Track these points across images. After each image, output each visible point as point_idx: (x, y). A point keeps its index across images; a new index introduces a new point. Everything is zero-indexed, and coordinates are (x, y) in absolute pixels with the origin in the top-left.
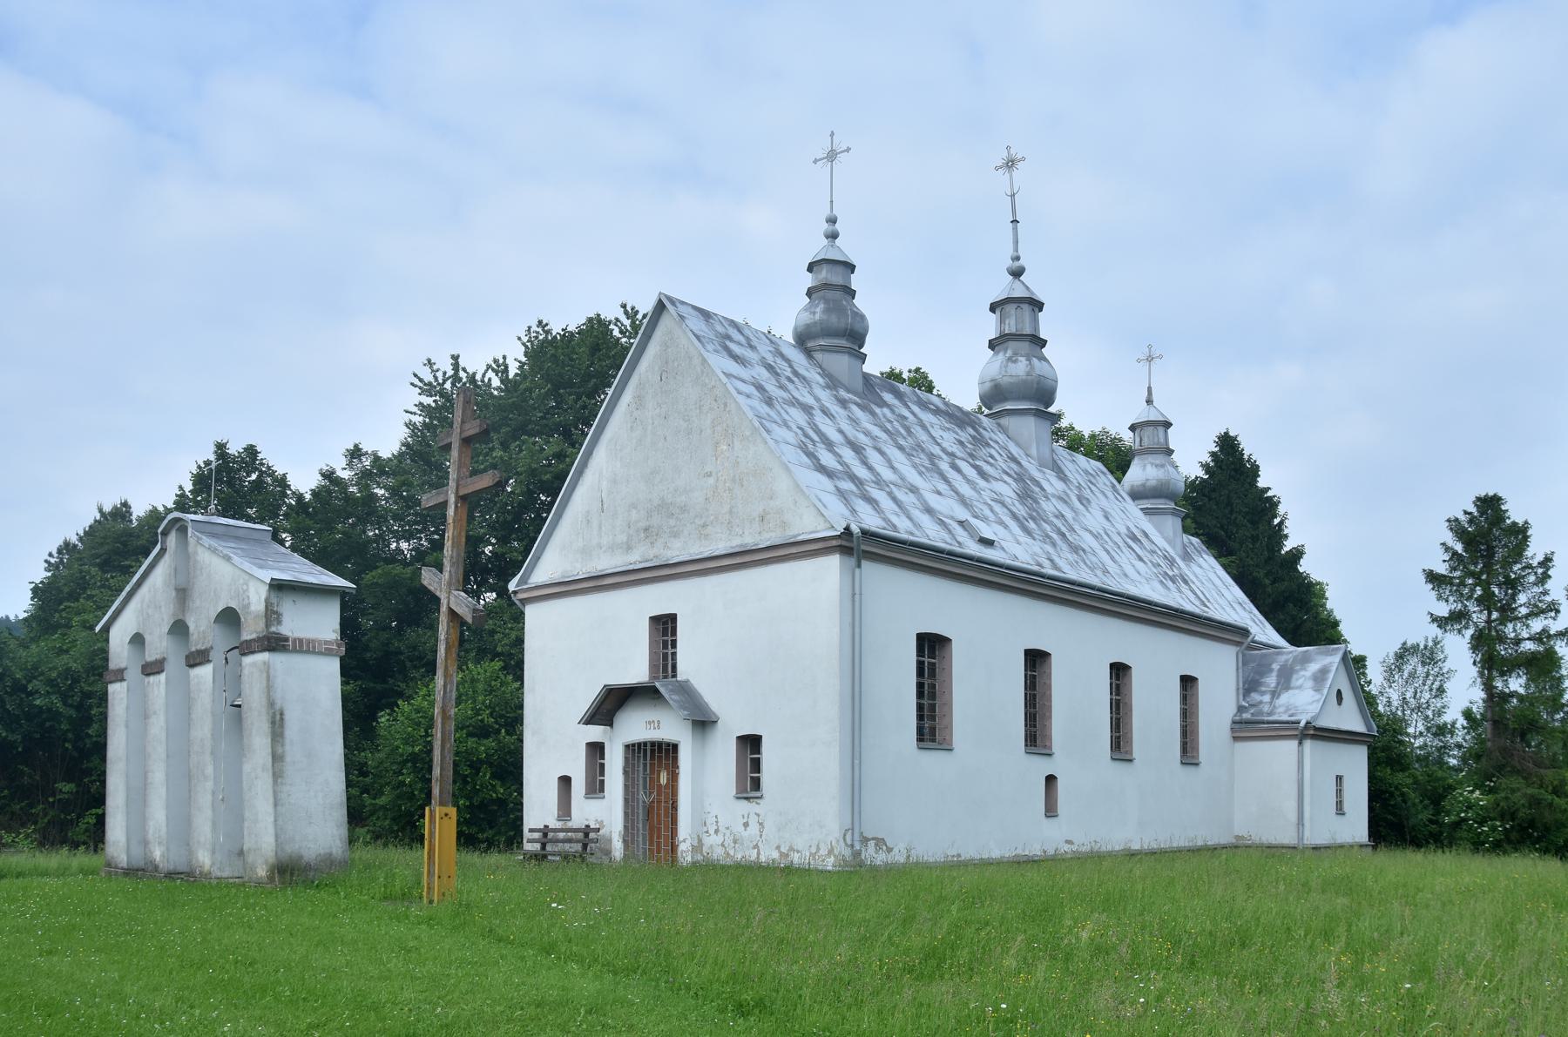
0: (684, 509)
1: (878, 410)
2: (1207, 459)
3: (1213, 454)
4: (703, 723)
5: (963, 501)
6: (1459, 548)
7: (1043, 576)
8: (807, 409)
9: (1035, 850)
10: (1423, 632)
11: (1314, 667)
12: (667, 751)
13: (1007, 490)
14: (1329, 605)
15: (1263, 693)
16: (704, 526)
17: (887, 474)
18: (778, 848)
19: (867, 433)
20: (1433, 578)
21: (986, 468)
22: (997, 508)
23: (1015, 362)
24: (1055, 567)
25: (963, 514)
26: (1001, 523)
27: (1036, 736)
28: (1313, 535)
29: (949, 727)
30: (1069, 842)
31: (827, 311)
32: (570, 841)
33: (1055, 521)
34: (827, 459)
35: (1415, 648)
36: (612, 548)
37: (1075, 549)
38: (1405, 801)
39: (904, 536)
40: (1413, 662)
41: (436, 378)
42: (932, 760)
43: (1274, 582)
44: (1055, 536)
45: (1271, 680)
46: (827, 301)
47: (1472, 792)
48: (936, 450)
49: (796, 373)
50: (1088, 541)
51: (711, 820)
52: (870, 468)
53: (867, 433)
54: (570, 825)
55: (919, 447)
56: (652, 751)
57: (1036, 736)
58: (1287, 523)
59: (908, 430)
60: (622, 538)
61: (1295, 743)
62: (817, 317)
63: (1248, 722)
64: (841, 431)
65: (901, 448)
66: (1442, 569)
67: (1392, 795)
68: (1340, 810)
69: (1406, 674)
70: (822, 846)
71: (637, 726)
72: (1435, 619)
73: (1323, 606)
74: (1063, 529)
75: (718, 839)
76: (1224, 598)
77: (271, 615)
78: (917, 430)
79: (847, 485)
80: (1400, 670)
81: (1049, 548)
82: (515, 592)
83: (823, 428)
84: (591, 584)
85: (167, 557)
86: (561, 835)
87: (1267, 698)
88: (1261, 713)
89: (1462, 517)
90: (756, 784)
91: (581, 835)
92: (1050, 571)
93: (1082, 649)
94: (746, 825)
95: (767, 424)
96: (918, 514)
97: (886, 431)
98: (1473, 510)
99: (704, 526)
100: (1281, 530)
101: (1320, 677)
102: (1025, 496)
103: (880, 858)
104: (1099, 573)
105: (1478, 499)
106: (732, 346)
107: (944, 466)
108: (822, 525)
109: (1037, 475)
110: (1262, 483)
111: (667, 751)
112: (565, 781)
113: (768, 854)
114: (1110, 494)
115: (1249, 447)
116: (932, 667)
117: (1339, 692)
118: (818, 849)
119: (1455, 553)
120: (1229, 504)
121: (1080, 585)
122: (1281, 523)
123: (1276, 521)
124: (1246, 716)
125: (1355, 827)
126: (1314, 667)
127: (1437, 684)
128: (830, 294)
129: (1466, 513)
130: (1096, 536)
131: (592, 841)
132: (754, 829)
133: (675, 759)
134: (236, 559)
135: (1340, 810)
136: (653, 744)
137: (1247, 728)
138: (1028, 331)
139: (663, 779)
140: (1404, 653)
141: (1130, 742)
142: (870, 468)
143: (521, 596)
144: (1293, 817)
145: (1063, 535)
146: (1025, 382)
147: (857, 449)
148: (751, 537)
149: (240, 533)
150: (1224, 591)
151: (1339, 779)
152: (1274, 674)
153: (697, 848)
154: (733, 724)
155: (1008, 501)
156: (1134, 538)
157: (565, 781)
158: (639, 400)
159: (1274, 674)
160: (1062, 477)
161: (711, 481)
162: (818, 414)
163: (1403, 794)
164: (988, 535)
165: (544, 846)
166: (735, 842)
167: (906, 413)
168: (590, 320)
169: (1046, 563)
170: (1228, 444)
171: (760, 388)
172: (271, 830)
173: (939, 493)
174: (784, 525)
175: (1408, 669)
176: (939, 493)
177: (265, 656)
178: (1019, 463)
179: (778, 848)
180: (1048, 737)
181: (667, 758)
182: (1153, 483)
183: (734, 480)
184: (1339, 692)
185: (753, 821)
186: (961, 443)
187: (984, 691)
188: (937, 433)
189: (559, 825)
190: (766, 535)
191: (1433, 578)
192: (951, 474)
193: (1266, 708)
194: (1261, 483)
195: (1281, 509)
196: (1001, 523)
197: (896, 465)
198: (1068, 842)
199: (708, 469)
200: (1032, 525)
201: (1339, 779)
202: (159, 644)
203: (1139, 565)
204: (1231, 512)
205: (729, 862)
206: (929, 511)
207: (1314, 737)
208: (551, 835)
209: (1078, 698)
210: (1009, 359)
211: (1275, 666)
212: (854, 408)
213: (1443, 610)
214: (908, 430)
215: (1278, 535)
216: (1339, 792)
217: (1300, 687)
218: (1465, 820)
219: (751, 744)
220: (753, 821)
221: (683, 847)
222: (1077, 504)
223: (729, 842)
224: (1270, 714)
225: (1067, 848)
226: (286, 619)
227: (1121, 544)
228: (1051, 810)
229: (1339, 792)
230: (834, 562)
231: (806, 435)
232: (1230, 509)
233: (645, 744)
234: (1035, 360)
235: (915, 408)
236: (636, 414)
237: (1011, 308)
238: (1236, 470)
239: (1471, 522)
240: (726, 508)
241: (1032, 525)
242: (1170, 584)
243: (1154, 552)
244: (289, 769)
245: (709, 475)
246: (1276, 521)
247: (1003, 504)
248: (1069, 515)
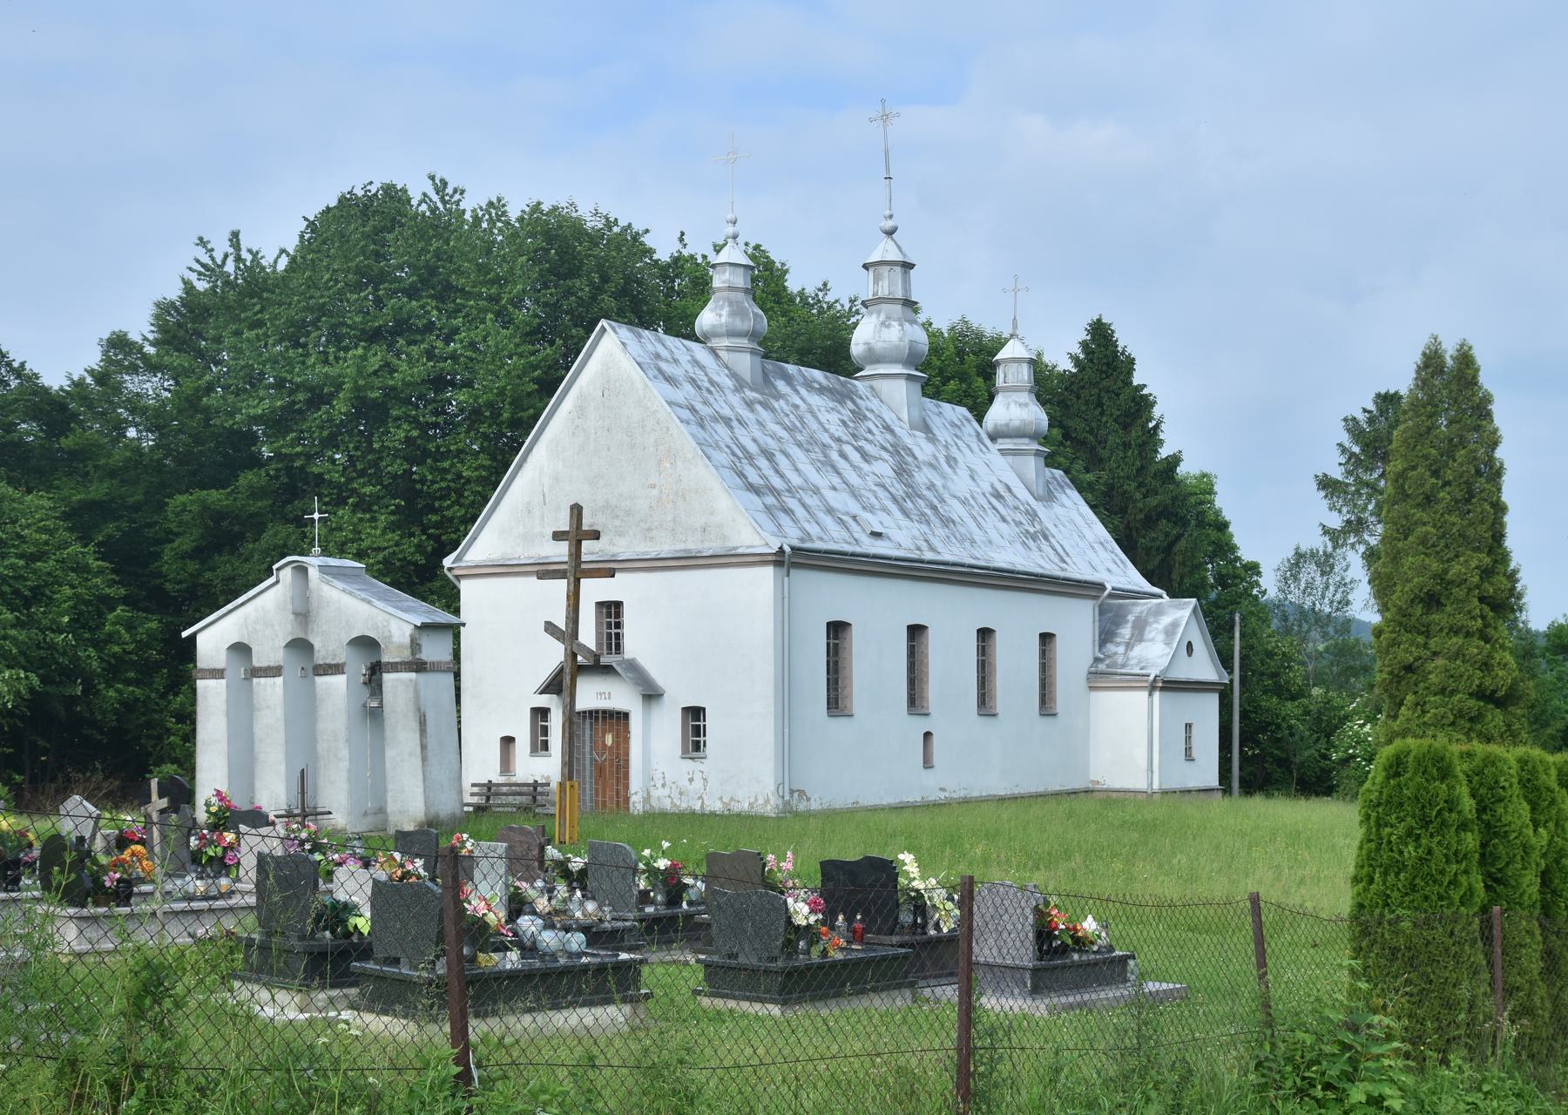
0: (629, 513)
1: (776, 405)
2: (1077, 350)
3: (1084, 345)
4: (651, 695)
5: (855, 494)
6: (1356, 449)
7: (922, 561)
8: (727, 422)
9: (914, 797)
10: (1316, 542)
11: (1166, 620)
13: (884, 468)
14: (1218, 503)
15: (1118, 644)
16: (649, 529)
17: (796, 480)
19: (773, 436)
20: (1327, 485)
21: (868, 448)
22: (881, 493)
23: (888, 326)
24: (932, 549)
25: (854, 507)
26: (885, 509)
27: (915, 700)
28: (1187, 437)
29: (850, 696)
30: (943, 789)
31: (732, 314)
32: (520, 794)
33: (926, 493)
34: (753, 477)
35: (1313, 554)
37: (947, 522)
38: (1292, 735)
39: (818, 545)
40: (1310, 571)
41: (213, 259)
43: (1145, 497)
44: (928, 512)
45: (1126, 632)
46: (731, 303)
47: (1362, 726)
48: (826, 439)
49: (711, 382)
50: (956, 510)
51: (658, 776)
52: (782, 476)
53: (773, 436)
54: (513, 780)
55: (813, 440)
57: (915, 700)
58: (1163, 426)
59: (801, 419)
61: (1146, 694)
62: (724, 319)
63: (1102, 673)
64: (754, 440)
65: (799, 445)
66: (1337, 473)
67: (1279, 727)
68: (1189, 756)
69: (1303, 585)
71: (591, 694)
72: (1326, 531)
73: (1211, 502)
74: (936, 502)
75: (666, 791)
76: (1085, 543)
77: (415, 646)
78: (808, 418)
79: (770, 500)
80: (1296, 579)
81: (924, 528)
82: (450, 569)
83: (742, 439)
85: (279, 586)
86: (505, 789)
87: (1121, 649)
88: (1114, 665)
89: (1361, 417)
90: (697, 747)
91: (485, 790)
92: (929, 556)
93: (953, 617)
94: (691, 780)
95: (710, 451)
96: (822, 516)
97: (786, 428)
98: (1371, 407)
99: (649, 529)
100: (1155, 433)
101: (1170, 631)
102: (902, 472)
103: (802, 807)
104: (967, 544)
105: (1378, 395)
106: (664, 366)
107: (835, 456)
108: (758, 542)
109: (908, 441)
110: (1137, 380)
112: (508, 741)
113: (715, 805)
114: (975, 446)
115: (1126, 339)
116: (836, 645)
117: (1190, 644)
119: (1353, 455)
120: (1100, 404)
121: (954, 564)
122: (1157, 427)
123: (1151, 425)
124: (1102, 667)
125: (1206, 772)
126: (1166, 620)
127: (1338, 596)
128: (733, 295)
129: (1365, 410)
130: (964, 502)
131: (542, 794)
132: (698, 783)
133: (627, 725)
134: (376, 603)
135: (1189, 756)
136: (604, 712)
137: (1101, 676)
138: (899, 295)
139: (609, 740)
140: (1300, 558)
141: (993, 698)
142: (782, 476)
143: (457, 572)
144: (1144, 764)
145: (934, 508)
146: (897, 347)
147: (769, 456)
148: (692, 544)
149: (348, 572)
150: (1086, 531)
151: (1188, 726)
152: (1129, 625)
153: (647, 799)
154: (678, 695)
155: (887, 482)
156: (998, 496)
157: (508, 741)
158: (581, 410)
159: (1129, 625)
160: (932, 439)
161: (655, 492)
162: (735, 424)
163: (1290, 727)
164: (878, 529)
165: (488, 799)
167: (798, 401)
168: (389, 189)
169: (924, 546)
170: (1100, 334)
171: (693, 410)
173: (834, 488)
174: (724, 538)
175: (1304, 577)
176: (834, 488)
177: (413, 675)
178: (892, 432)
180: (923, 698)
182: (1016, 423)
183: (677, 494)
184: (1190, 644)
185: (698, 776)
186: (844, 422)
187: (877, 664)
188: (824, 416)
189: (502, 780)
190: (707, 545)
191: (1327, 485)
192: (841, 464)
193: (1120, 660)
194: (1137, 380)
195: (1157, 412)
196: (885, 509)
197: (800, 466)
198: (943, 789)
199: (651, 481)
200: (909, 505)
201: (1188, 726)
202: (269, 651)
203: (1003, 526)
204: (1102, 414)
205: (675, 810)
206: (830, 511)
207: (1162, 689)
209: (951, 662)
210: (883, 324)
211: (1131, 618)
212: (758, 407)
213: (1336, 521)
214: (801, 419)
215: (1151, 438)
216: (1188, 739)
217: (1152, 640)
218: (1353, 757)
219: (694, 715)
220: (698, 776)
221: (633, 799)
222: (945, 467)
223: (675, 795)
224: (1123, 666)
225: (942, 795)
226: (424, 649)
227: (986, 506)
228: (928, 763)
229: (1188, 739)
230: (769, 571)
231: (734, 454)
232: (1098, 421)
233: (597, 712)
234: (907, 325)
235: (803, 391)
236: (577, 422)
237: (885, 270)
238: (1108, 365)
239: (1371, 421)
240: (669, 518)
241: (909, 505)
242: (1031, 543)
243: (1016, 508)
244: (430, 754)
245: (654, 486)
246: (1151, 425)
247: (883, 486)
248: (938, 483)
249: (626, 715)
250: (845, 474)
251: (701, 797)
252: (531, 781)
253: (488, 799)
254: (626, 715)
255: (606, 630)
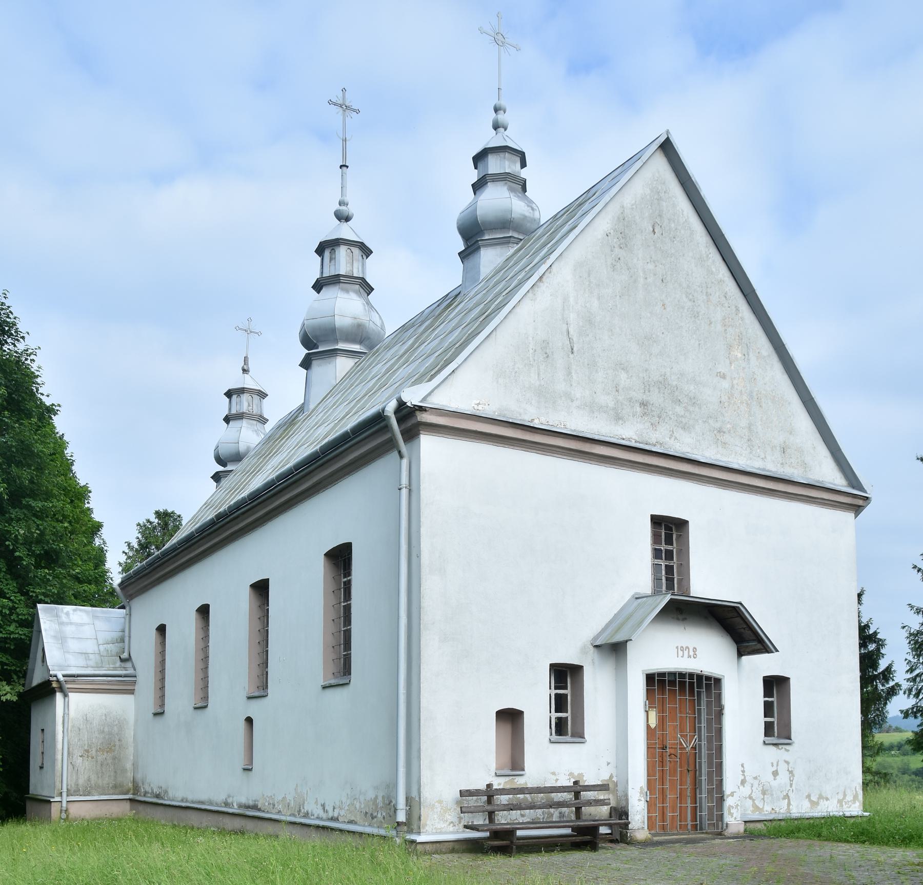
0: (693, 401)
12: (682, 684)
18: (809, 796)
32: (532, 807)
36: (592, 408)
42: (320, 688)
54: (520, 782)
56: (691, 684)
60: (607, 400)
70: (849, 792)
75: (746, 791)
84: (587, 447)
91: (568, 796)
94: (775, 774)
99: (720, 431)
111: (708, 687)
112: (510, 718)
118: (845, 795)
132: (783, 777)
161: (725, 384)
165: (491, 815)
166: (764, 792)
172: (844, 846)
174: (805, 465)
179: (809, 796)
181: (709, 694)
185: (782, 769)
199: (721, 369)
208: (587, 795)
220: (782, 769)
223: (757, 794)
233: (682, 675)
245: (724, 377)
249: (718, 681)
250: (62, 714)
251: (787, 797)
252: (482, 786)
253: (491, 815)
254: (718, 681)
255: (674, 548)
